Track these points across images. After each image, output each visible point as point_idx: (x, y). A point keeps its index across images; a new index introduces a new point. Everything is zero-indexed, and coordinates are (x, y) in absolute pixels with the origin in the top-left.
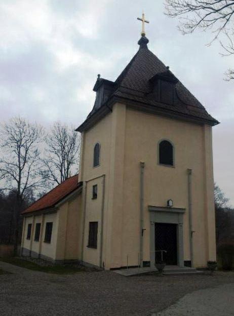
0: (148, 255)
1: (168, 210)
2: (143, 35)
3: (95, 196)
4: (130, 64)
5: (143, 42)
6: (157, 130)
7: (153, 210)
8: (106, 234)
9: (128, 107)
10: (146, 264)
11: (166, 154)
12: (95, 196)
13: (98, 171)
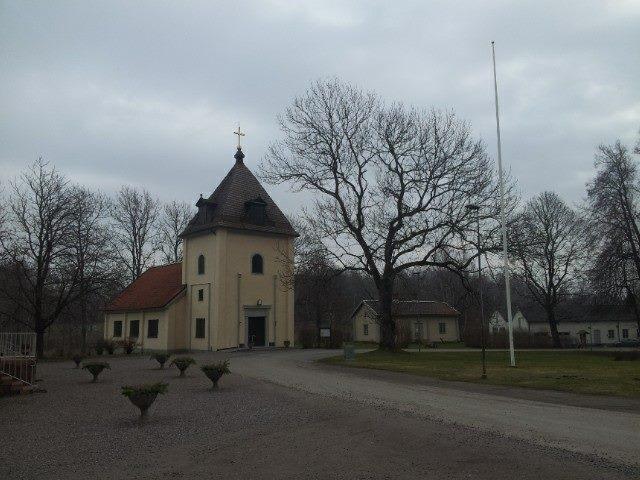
0: (243, 339)
1: (258, 307)
2: (239, 149)
3: (201, 297)
4: (231, 174)
5: (239, 156)
6: (248, 246)
7: (247, 308)
8: (213, 326)
9: (229, 232)
10: (241, 346)
11: (257, 265)
12: (201, 297)
13: (204, 279)
